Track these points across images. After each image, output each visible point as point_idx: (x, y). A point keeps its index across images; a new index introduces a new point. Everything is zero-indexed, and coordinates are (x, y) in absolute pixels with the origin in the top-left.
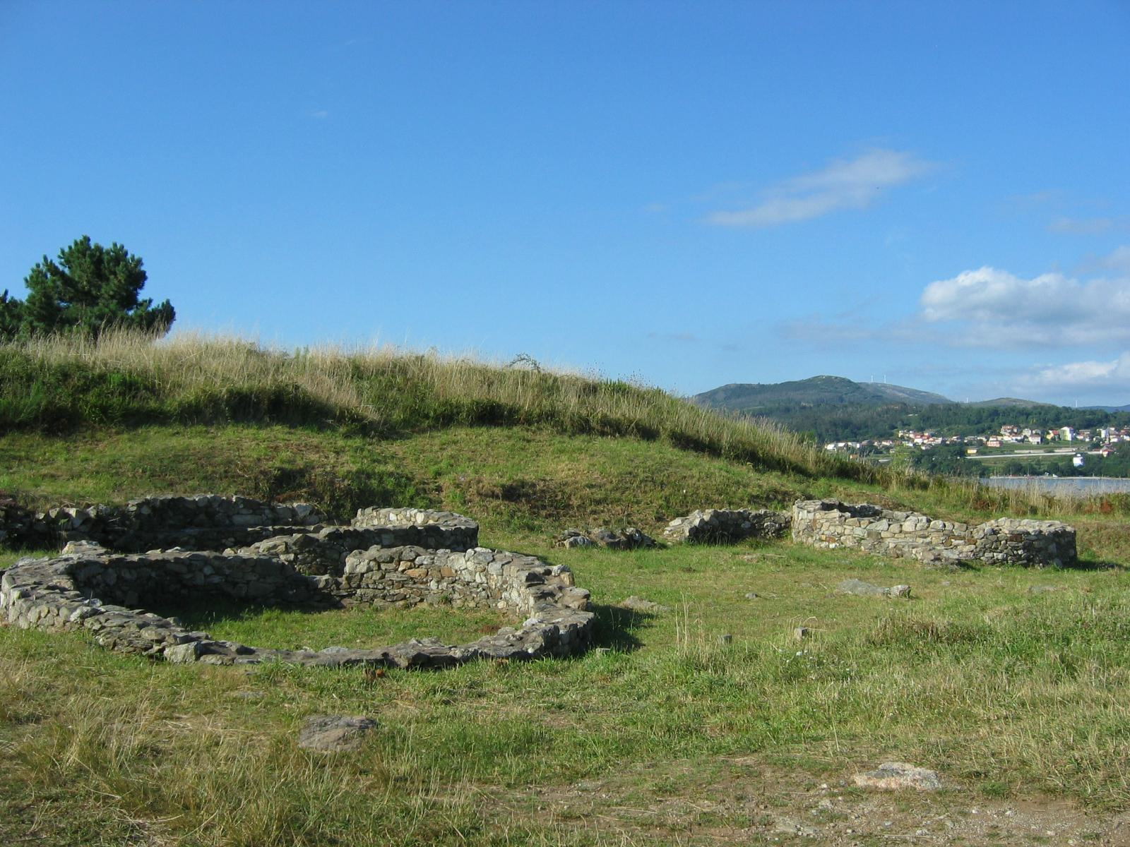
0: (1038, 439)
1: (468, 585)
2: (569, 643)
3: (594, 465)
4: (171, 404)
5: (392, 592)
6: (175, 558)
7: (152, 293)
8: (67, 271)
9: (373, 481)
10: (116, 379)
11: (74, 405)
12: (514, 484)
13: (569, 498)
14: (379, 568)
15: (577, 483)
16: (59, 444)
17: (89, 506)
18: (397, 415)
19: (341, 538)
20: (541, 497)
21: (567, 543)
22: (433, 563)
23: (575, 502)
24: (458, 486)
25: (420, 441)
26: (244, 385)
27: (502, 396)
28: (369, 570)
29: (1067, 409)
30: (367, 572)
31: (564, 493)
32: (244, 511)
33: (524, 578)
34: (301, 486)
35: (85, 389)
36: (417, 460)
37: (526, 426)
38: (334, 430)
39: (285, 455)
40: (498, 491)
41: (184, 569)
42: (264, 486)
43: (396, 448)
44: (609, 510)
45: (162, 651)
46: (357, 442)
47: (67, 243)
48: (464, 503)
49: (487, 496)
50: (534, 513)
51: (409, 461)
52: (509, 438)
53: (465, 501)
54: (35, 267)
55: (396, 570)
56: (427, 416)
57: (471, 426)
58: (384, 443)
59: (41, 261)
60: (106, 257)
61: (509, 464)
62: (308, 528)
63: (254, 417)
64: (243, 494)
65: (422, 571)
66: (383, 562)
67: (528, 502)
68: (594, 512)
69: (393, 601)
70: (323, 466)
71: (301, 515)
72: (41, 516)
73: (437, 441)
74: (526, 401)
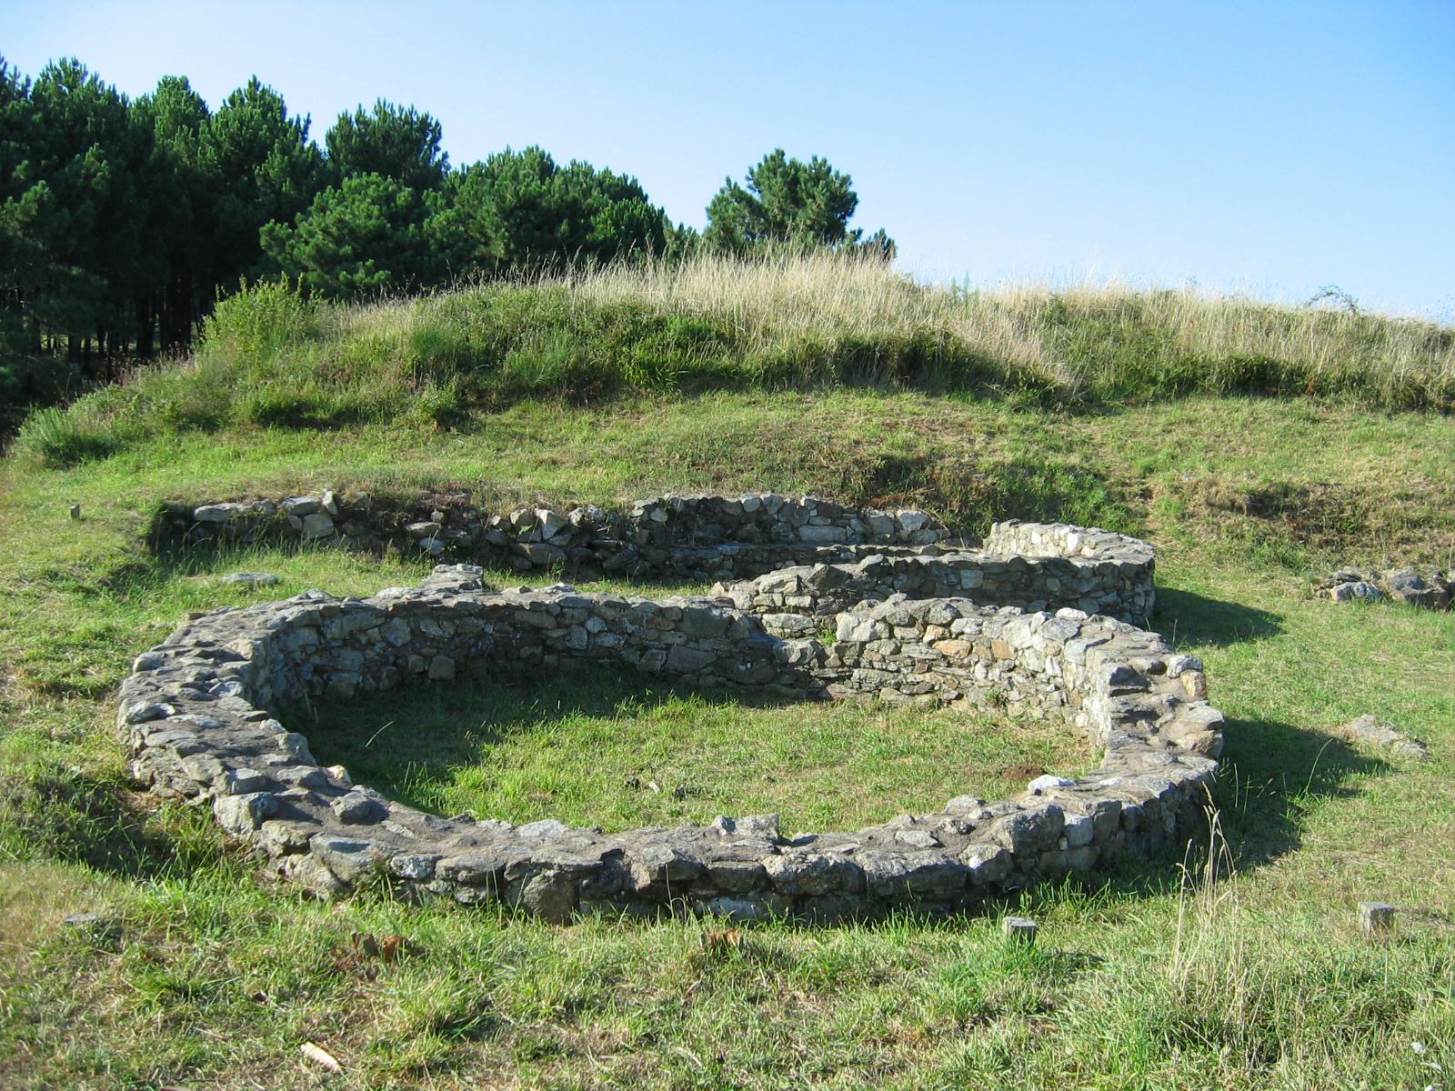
1: (1033, 676)
2: (1092, 843)
3: (1417, 462)
4: (751, 362)
5: (911, 678)
7: (862, 221)
8: (756, 196)
9: (1036, 479)
10: (676, 326)
11: (614, 361)
12: (1271, 490)
13: (1365, 515)
14: (891, 636)
15: (1381, 490)
16: (587, 417)
17: (574, 507)
18: (1103, 379)
19: (891, 574)
20: (1315, 512)
21: (1334, 592)
22: (981, 632)
23: (1374, 522)
24: (1176, 490)
25: (1138, 419)
26: (865, 333)
27: (1283, 352)
28: (875, 637)
30: (871, 641)
31: (1355, 505)
32: (818, 521)
33: (1108, 678)
34: (916, 484)
35: (630, 341)
36: (1121, 448)
37: (1316, 397)
38: (997, 399)
39: (902, 435)
40: (1241, 500)
41: (548, 622)
42: (857, 482)
43: (1082, 428)
44: (1432, 538)
45: (209, 802)
46: (1033, 418)
47: (755, 160)
48: (1183, 517)
49: (1221, 507)
50: (1301, 535)
51: (1108, 449)
52: (1284, 415)
53: (1183, 515)
54: (719, 193)
55: (919, 640)
56: (1153, 381)
57: (1224, 396)
58: (1076, 421)
59: (724, 184)
60: (803, 176)
61: (1272, 458)
62: (915, 549)
63: (877, 383)
64: (821, 493)
65: (962, 644)
66: (898, 625)
67: (1292, 519)
68: (1405, 540)
69: (912, 695)
70: (960, 454)
71: (908, 528)
72: (496, 521)
73: (1162, 419)
74: (1319, 358)
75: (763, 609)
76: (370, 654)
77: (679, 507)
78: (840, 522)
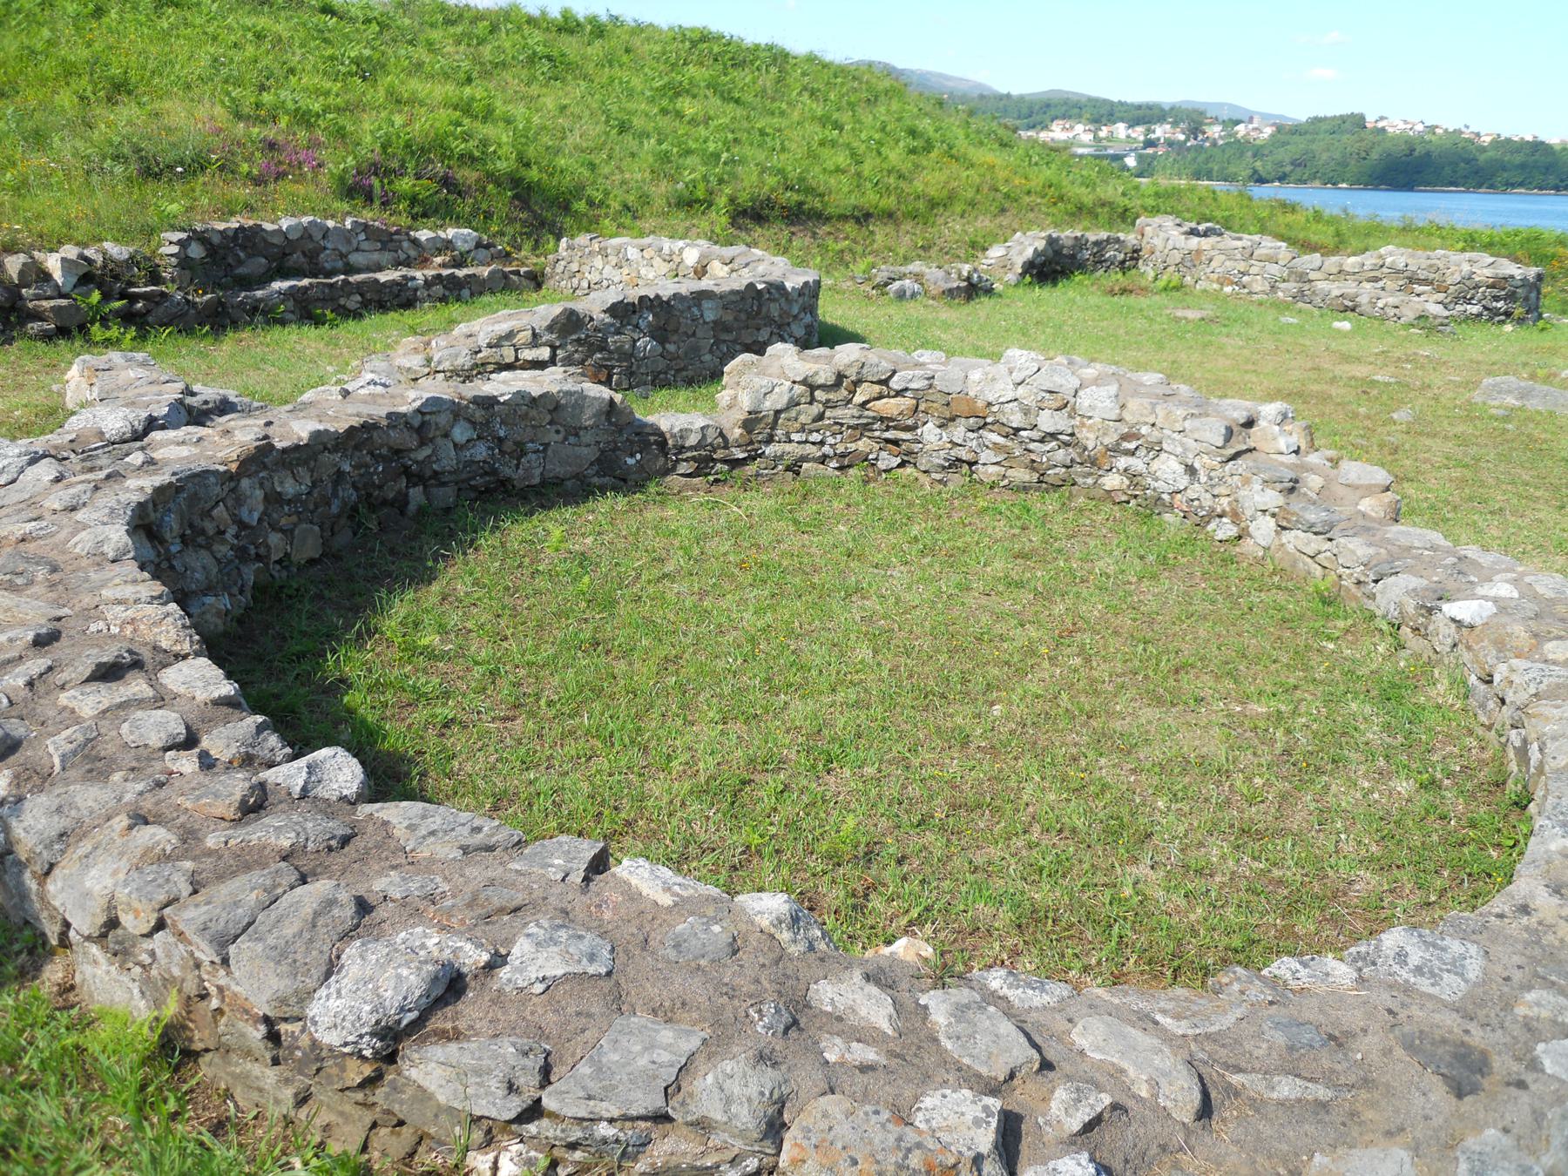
0: (1091, 136)
5: (840, 449)
6: (389, 416)
29: (1121, 103)
32: (365, 246)
65: (906, 402)
75: (491, 367)
76: (223, 550)
77: (216, 240)
78: (390, 245)
